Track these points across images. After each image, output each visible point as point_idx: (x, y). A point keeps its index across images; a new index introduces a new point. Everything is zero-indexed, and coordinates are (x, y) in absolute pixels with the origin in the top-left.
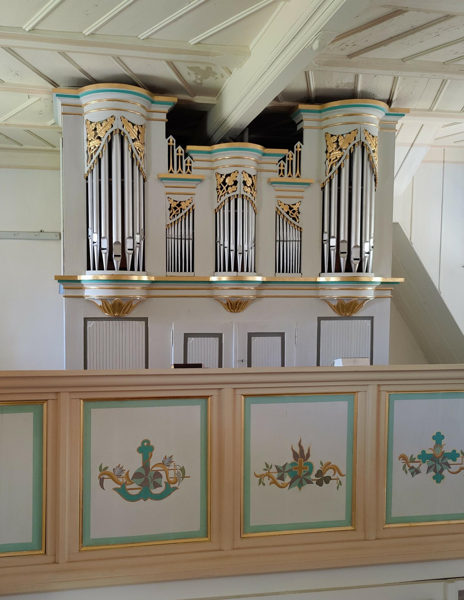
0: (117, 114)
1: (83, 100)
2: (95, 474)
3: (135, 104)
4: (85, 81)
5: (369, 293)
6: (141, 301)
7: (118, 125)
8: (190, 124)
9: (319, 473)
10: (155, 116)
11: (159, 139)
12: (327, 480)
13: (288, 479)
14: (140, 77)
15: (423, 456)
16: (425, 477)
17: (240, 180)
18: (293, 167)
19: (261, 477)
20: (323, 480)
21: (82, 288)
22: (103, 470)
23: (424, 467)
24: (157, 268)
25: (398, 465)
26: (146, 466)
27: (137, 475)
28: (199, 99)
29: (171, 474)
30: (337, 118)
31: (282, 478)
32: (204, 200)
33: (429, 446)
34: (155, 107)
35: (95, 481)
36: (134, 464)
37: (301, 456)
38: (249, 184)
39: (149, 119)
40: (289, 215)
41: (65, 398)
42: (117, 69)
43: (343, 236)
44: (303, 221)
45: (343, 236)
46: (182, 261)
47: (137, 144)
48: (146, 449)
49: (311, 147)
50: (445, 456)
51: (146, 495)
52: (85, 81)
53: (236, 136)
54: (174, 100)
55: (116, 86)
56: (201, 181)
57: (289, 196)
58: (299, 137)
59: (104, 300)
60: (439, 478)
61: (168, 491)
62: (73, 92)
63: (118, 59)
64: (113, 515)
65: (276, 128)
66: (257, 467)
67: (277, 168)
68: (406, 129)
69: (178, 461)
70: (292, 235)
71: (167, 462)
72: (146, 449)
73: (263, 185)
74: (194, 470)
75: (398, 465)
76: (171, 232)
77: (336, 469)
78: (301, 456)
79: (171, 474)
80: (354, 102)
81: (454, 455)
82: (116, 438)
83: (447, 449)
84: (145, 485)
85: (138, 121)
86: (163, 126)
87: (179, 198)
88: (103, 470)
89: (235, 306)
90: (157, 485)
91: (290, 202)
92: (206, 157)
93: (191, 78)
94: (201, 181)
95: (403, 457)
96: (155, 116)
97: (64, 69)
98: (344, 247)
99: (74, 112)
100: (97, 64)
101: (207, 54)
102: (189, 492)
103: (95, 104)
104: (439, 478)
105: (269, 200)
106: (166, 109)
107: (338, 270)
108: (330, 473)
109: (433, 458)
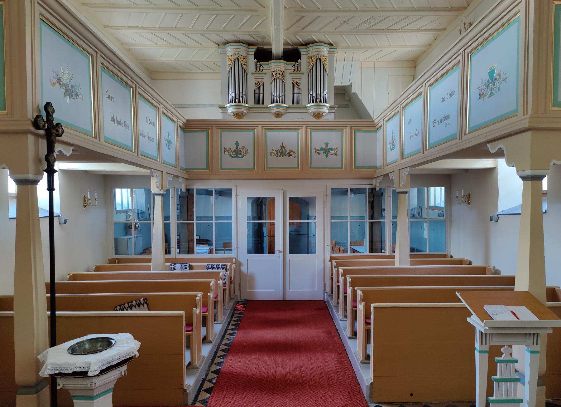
0: (236, 53)
1: (227, 49)
2: (223, 150)
3: (242, 50)
4: (226, 43)
5: (325, 110)
6: (246, 114)
7: (237, 56)
8: (263, 55)
9: (288, 153)
10: (250, 53)
11: (251, 61)
12: (291, 155)
13: (279, 154)
14: (245, 41)
15: (322, 149)
16: (323, 156)
17: (278, 72)
18: (298, 68)
19: (271, 153)
20: (290, 155)
21: (227, 110)
22: (225, 149)
23: (322, 152)
24: (251, 102)
25: (313, 151)
26: (237, 149)
27: (234, 151)
28: (266, 47)
29: (244, 151)
30: (312, 50)
31: (277, 154)
32: (267, 80)
33: (323, 146)
34: (250, 50)
35: (223, 152)
36: (234, 148)
37: (283, 147)
38: (281, 73)
39: (248, 54)
40: (296, 85)
41: (214, 128)
42: (234, 38)
43: (318, 92)
44: (302, 87)
45: (318, 92)
46: (260, 101)
47: (244, 62)
48: (237, 144)
49: (304, 61)
50: (329, 149)
51: (237, 157)
52: (226, 43)
53: (278, 58)
54: (256, 47)
55: (236, 44)
56: (266, 74)
57: (296, 77)
58: (300, 58)
59: (233, 113)
60: (327, 156)
61: (243, 156)
62: (223, 47)
63: (234, 35)
64: (229, 162)
65: (292, 55)
66: (270, 150)
67: (292, 69)
68: (339, 54)
69: (246, 147)
70: (298, 91)
71: (243, 148)
72: (237, 144)
73: (287, 75)
74: (251, 150)
75: (313, 151)
76: (256, 92)
77: (294, 152)
78: (283, 147)
79: (244, 151)
80: (316, 44)
81: (332, 149)
82: (229, 140)
83: (330, 147)
84: (237, 154)
85: (244, 55)
86: (253, 56)
87: (259, 80)
88: (225, 149)
89: (278, 115)
90: (240, 154)
91: (297, 80)
92: (267, 66)
93: (259, 40)
94: (266, 74)
95: (315, 149)
96: (250, 53)
97: (220, 40)
98: (318, 96)
99: (225, 53)
100: (229, 37)
101: (258, 32)
102: (249, 156)
103: (230, 50)
104: (327, 156)
105: (289, 80)
106: (254, 50)
107: (313, 102)
108: (292, 153)
109: (325, 150)
